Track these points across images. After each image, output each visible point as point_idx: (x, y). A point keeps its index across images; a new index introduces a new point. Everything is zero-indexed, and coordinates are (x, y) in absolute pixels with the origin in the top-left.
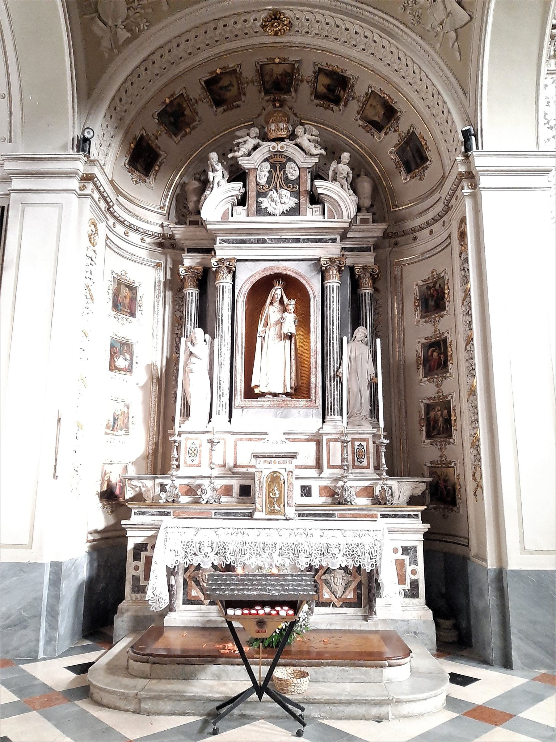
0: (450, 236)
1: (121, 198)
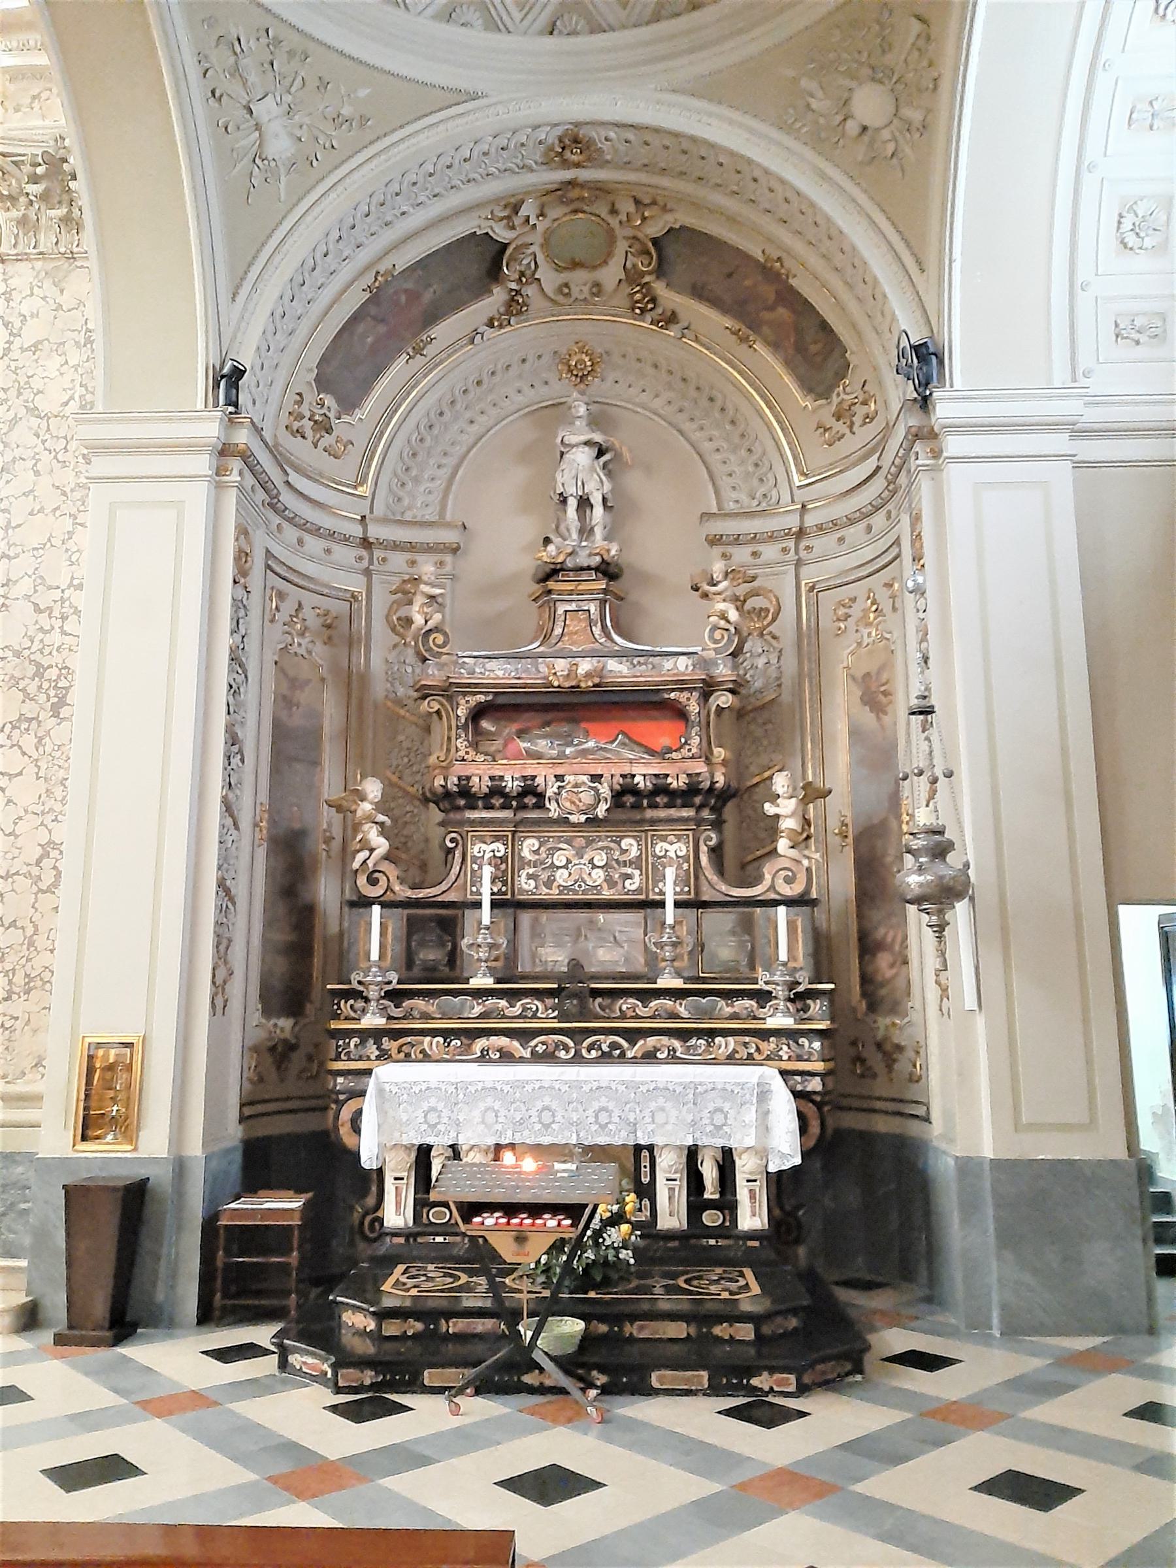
0: (897, 542)
1: (293, 477)
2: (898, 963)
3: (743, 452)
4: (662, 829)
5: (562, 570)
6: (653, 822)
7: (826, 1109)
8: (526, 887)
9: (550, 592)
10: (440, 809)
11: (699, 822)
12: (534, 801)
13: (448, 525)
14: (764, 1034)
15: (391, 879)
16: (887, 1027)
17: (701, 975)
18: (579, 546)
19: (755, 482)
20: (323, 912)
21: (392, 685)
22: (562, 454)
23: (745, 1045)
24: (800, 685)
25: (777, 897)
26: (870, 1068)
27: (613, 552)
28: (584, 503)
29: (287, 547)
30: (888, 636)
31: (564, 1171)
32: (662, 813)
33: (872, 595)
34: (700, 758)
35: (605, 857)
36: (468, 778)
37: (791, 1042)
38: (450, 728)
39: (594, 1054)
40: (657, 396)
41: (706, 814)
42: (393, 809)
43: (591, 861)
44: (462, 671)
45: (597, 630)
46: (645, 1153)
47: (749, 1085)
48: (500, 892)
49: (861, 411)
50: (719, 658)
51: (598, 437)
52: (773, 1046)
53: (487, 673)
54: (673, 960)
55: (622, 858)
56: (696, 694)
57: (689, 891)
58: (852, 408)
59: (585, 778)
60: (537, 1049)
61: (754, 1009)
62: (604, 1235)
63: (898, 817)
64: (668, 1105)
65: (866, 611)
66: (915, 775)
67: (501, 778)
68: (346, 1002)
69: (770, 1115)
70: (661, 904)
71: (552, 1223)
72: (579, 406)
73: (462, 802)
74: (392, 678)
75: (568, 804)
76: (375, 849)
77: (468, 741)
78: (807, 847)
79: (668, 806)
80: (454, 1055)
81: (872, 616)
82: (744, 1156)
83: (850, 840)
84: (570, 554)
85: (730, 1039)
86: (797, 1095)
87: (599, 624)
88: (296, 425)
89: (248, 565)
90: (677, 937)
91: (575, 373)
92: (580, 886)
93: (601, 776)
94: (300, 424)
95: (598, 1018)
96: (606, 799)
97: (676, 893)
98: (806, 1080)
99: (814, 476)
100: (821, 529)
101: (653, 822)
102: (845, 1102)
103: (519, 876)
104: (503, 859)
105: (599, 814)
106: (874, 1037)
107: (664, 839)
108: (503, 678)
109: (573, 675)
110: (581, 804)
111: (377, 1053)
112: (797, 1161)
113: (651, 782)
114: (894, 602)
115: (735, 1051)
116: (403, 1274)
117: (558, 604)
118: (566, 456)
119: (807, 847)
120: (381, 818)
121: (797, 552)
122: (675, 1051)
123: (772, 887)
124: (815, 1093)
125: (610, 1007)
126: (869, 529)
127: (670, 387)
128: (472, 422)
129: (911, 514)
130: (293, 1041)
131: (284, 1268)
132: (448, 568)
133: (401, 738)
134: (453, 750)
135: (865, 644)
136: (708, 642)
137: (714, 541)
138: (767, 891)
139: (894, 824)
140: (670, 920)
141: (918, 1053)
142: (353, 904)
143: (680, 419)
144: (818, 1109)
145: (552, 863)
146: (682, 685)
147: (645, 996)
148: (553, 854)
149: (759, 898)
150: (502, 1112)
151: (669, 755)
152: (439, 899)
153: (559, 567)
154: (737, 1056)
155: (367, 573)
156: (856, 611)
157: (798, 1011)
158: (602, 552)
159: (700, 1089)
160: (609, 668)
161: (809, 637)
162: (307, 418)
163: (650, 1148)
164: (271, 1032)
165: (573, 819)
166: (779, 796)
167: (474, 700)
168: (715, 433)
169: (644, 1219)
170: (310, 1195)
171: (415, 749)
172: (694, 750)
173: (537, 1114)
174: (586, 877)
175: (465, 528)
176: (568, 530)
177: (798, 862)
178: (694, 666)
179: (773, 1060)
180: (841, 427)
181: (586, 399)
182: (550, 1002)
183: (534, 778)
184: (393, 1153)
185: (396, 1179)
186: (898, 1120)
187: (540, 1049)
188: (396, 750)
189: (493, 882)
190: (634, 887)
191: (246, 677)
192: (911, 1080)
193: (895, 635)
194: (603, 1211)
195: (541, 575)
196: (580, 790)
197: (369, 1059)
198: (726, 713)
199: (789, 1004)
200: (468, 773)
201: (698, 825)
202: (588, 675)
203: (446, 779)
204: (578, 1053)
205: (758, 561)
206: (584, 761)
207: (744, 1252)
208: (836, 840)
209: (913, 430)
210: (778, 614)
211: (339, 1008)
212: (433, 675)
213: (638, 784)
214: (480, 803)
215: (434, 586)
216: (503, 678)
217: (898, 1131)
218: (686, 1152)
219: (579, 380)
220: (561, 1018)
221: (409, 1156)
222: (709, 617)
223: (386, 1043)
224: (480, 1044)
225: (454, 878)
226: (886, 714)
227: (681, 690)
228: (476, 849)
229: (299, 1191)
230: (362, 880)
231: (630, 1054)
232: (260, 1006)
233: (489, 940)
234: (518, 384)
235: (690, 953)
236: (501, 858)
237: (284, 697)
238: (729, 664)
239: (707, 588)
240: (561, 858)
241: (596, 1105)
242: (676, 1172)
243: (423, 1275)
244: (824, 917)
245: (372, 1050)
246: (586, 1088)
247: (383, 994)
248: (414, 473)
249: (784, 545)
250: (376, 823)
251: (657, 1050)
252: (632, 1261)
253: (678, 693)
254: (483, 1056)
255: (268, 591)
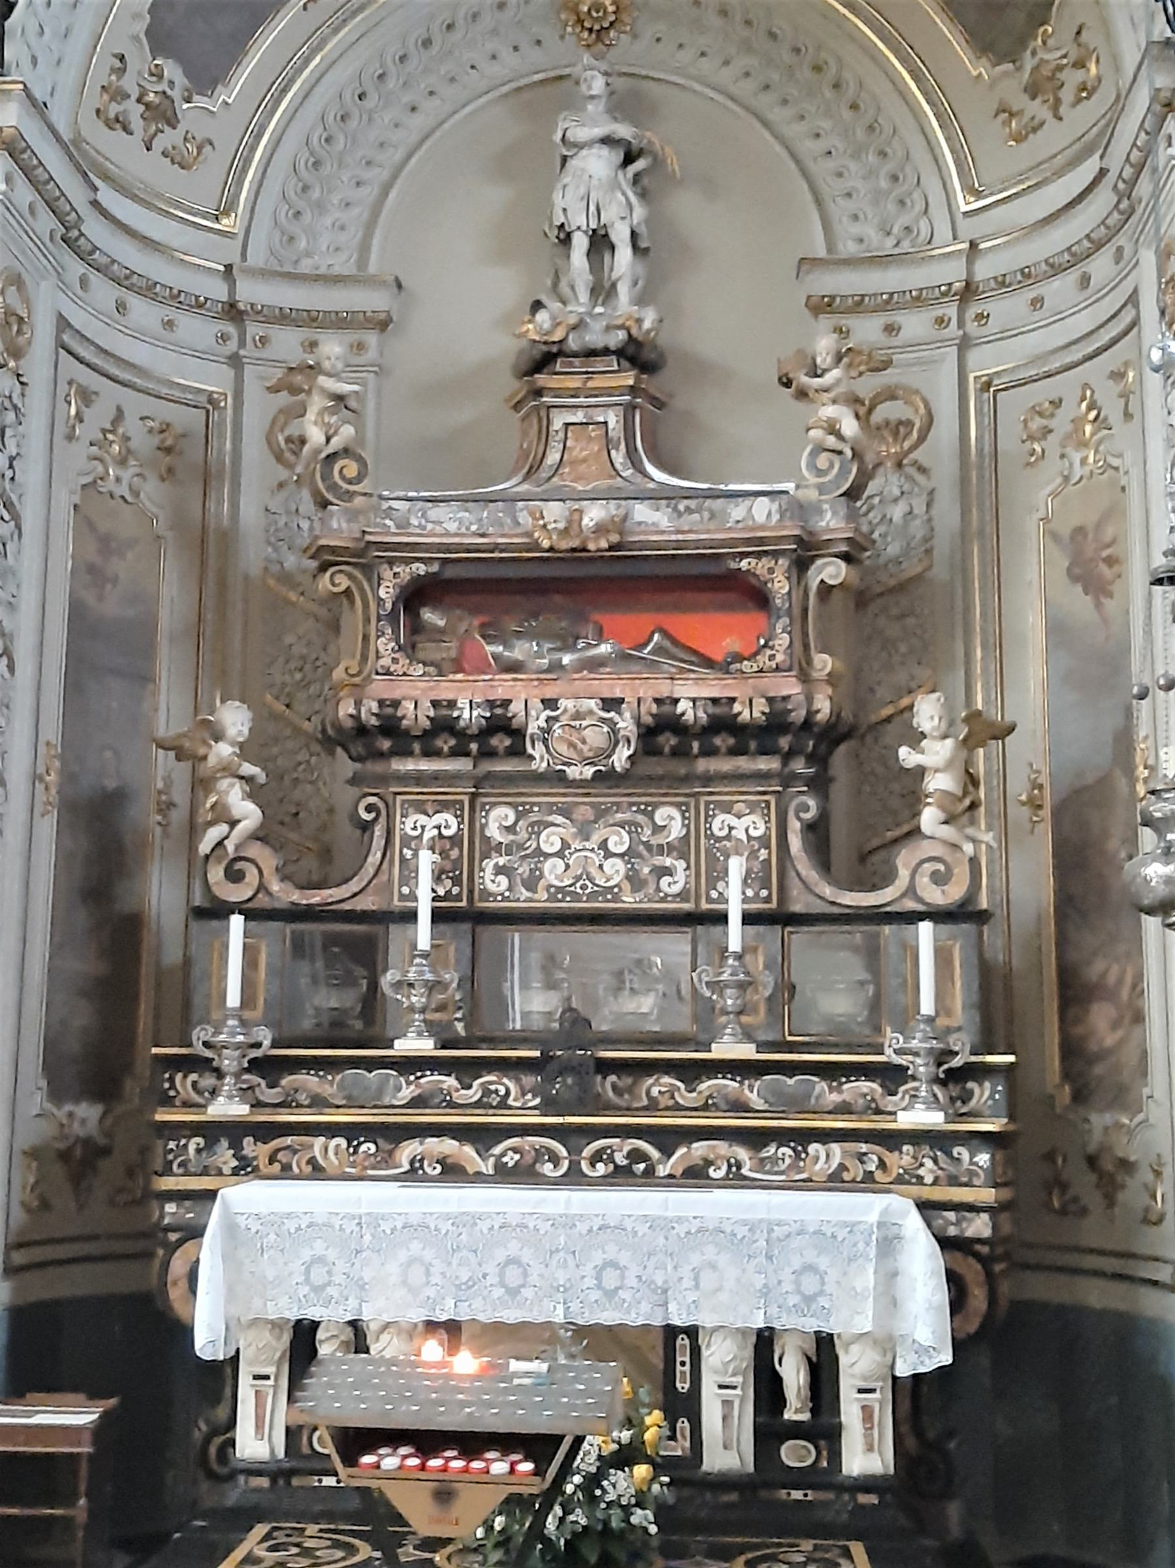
0: (1133, 299)
1: (107, 196)
2: (1127, 1021)
3: (872, 158)
4: (724, 792)
5: (560, 353)
6: (708, 779)
7: (998, 1268)
8: (492, 887)
9: (539, 393)
10: (350, 757)
11: (787, 780)
12: (508, 742)
13: (372, 282)
14: (892, 1140)
15: (265, 873)
16: (1106, 1129)
17: (790, 1038)
18: (590, 314)
19: (891, 207)
20: (154, 926)
21: (276, 550)
22: (565, 159)
23: (861, 1157)
24: (966, 557)
25: (920, 908)
26: (1075, 1200)
27: (647, 325)
28: (600, 242)
29: (98, 314)
30: (1115, 462)
31: (527, 1374)
32: (725, 765)
33: (1088, 393)
34: (790, 670)
35: (626, 837)
36: (396, 704)
37: (939, 1153)
38: (367, 620)
39: (601, 1169)
40: (726, 63)
41: (799, 766)
42: (276, 758)
43: (603, 845)
44: (388, 522)
45: (619, 457)
46: (683, 1341)
47: (862, 1227)
48: (448, 896)
49: (1072, 78)
50: (826, 502)
51: (624, 131)
52: (906, 1160)
53: (430, 526)
54: (740, 1013)
55: (654, 841)
56: (783, 562)
57: (770, 895)
58: (1058, 75)
59: (592, 704)
60: (505, 1159)
61: (877, 1097)
62: (605, 1483)
63: (1129, 771)
64: (723, 1260)
65: (1078, 422)
66: (1160, 688)
67: (452, 704)
68: (185, 1077)
69: (899, 1277)
70: (721, 918)
71: (499, 1468)
72: (593, 77)
73: (386, 744)
74: (276, 538)
75: (563, 749)
76: (239, 821)
77: (398, 643)
78: (973, 822)
79: (735, 752)
80: (366, 1168)
81: (1088, 429)
82: (855, 1348)
83: (1046, 812)
84: (574, 328)
85: (836, 1148)
86: (946, 1243)
87: (623, 446)
88: (114, 109)
89: (21, 340)
90: (747, 973)
91: (587, 25)
92: (584, 887)
93: (622, 700)
94: (120, 108)
95: (608, 1108)
96: (629, 742)
97: (745, 900)
98: (964, 1218)
99: (992, 194)
100: (1003, 284)
101: (708, 779)
102: (1031, 1256)
103: (483, 870)
104: (455, 840)
105: (616, 764)
106: (1085, 1145)
107: (727, 808)
108: (456, 535)
109: (575, 530)
110: (585, 748)
111: (235, 1163)
112: (946, 1358)
113: (705, 712)
114: (1127, 405)
115: (842, 1167)
116: (259, 1543)
117: (552, 410)
118: (572, 164)
119: (973, 822)
120: (248, 769)
121: (961, 324)
122: (739, 1166)
123: (911, 891)
124: (980, 1241)
125: (630, 1090)
126: (1085, 281)
127: (747, 47)
128: (413, 109)
129: (1158, 247)
130: (102, 1141)
131: (67, 1522)
132: (371, 354)
133: (289, 639)
134: (372, 655)
135: (1077, 479)
136: (805, 472)
137: (822, 306)
138: (903, 895)
139: (1122, 783)
140: (735, 944)
141: (1158, 1174)
142: (200, 913)
143: (764, 102)
144: (984, 1266)
145: (538, 847)
146: (760, 547)
147: (690, 1072)
148: (539, 834)
149: (888, 909)
150: (438, 1267)
151: (738, 665)
152: (346, 906)
153: (555, 349)
154: (846, 1176)
155: (235, 361)
156: (1061, 423)
157: (952, 1100)
158: (628, 323)
159: (778, 1232)
160: (638, 517)
161: (980, 467)
162: (134, 98)
163: (692, 1332)
164: (62, 1125)
165: (573, 772)
166: (923, 736)
167: (405, 572)
168: (825, 124)
169: (679, 1453)
170: (113, 1402)
171: (314, 656)
172: (780, 658)
173: (497, 1270)
174: (594, 871)
175: (399, 286)
176: (573, 288)
177: (956, 847)
178: (782, 513)
179: (909, 1183)
180: (1037, 109)
181: (604, 67)
182: (529, 1080)
183: (506, 703)
184: (252, 1334)
185: (256, 1377)
186: (1122, 1287)
187: (511, 1159)
188: (281, 660)
189: (437, 879)
190: (676, 889)
191: (18, 527)
192: (1146, 1221)
193: (1129, 456)
194: (594, 1447)
195: (524, 368)
196: (584, 723)
197: (220, 1173)
198: (836, 596)
199: (936, 1089)
200: (396, 695)
201: (786, 785)
202: (600, 529)
203: (358, 704)
204: (574, 1168)
205: (895, 342)
206: (592, 676)
207: (852, 1512)
208: (1019, 814)
209: (1163, 94)
210: (929, 430)
211: (173, 1086)
212: (340, 530)
213: (683, 714)
214: (417, 747)
215: (340, 380)
216: (456, 535)
217: (1122, 1306)
218: (754, 1339)
219: (594, 36)
220: (548, 1107)
221: (279, 1338)
222: (808, 430)
223: (249, 1146)
224: (409, 1150)
225: (372, 871)
226: (1110, 595)
227: (759, 555)
228: (410, 823)
229: (94, 1394)
230: (216, 874)
231: (662, 1171)
232: (43, 1083)
233: (429, 976)
234: (490, 46)
235: (769, 999)
236: (450, 838)
237: (92, 569)
238: (843, 511)
239: (805, 379)
240: (552, 839)
241: (598, 1258)
242: (734, 1375)
243: (297, 1545)
244: (1000, 943)
245: (225, 1157)
246: (582, 1228)
247: (246, 1065)
248: (316, 194)
249: (940, 313)
250: (242, 778)
251: (708, 1163)
252: (653, 1529)
253: (754, 561)
254: (413, 1170)
255: (62, 388)
